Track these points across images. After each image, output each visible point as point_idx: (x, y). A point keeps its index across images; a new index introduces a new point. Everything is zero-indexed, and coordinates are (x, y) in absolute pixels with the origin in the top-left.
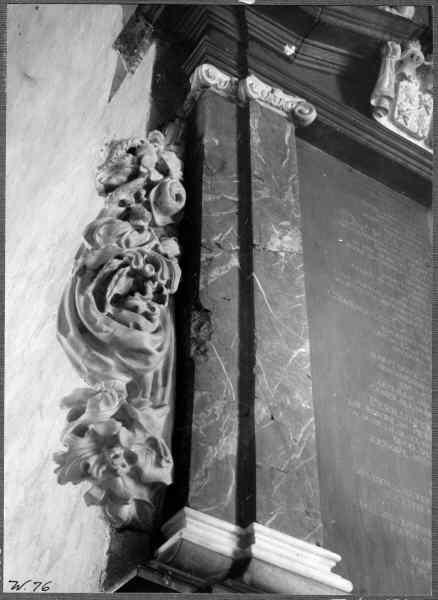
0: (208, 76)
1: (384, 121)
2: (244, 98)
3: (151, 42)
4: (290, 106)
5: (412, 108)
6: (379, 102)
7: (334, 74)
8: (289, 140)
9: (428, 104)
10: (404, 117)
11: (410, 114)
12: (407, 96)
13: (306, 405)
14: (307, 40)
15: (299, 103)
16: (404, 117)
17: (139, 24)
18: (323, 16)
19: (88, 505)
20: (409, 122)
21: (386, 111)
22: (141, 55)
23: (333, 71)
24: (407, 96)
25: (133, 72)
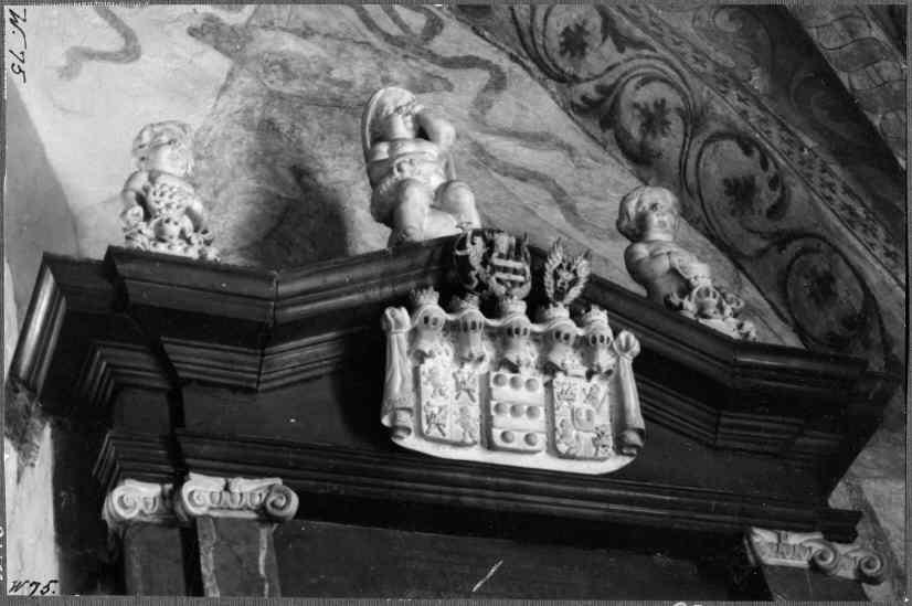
0: (124, 507)
1: (410, 442)
2: (186, 519)
3: (44, 423)
4: (257, 500)
5: (448, 402)
6: (394, 419)
7: (326, 374)
8: (267, 568)
9: (469, 385)
10: (438, 425)
11: (444, 418)
12: (435, 385)
13: (833, 319)
14: (267, 350)
15: (270, 487)
16: (438, 425)
17: (20, 395)
18: (279, 313)
19: (726, 181)
20: (446, 430)
21: (408, 431)
22: (35, 441)
23: (323, 371)
24: (435, 385)
25: (33, 465)
